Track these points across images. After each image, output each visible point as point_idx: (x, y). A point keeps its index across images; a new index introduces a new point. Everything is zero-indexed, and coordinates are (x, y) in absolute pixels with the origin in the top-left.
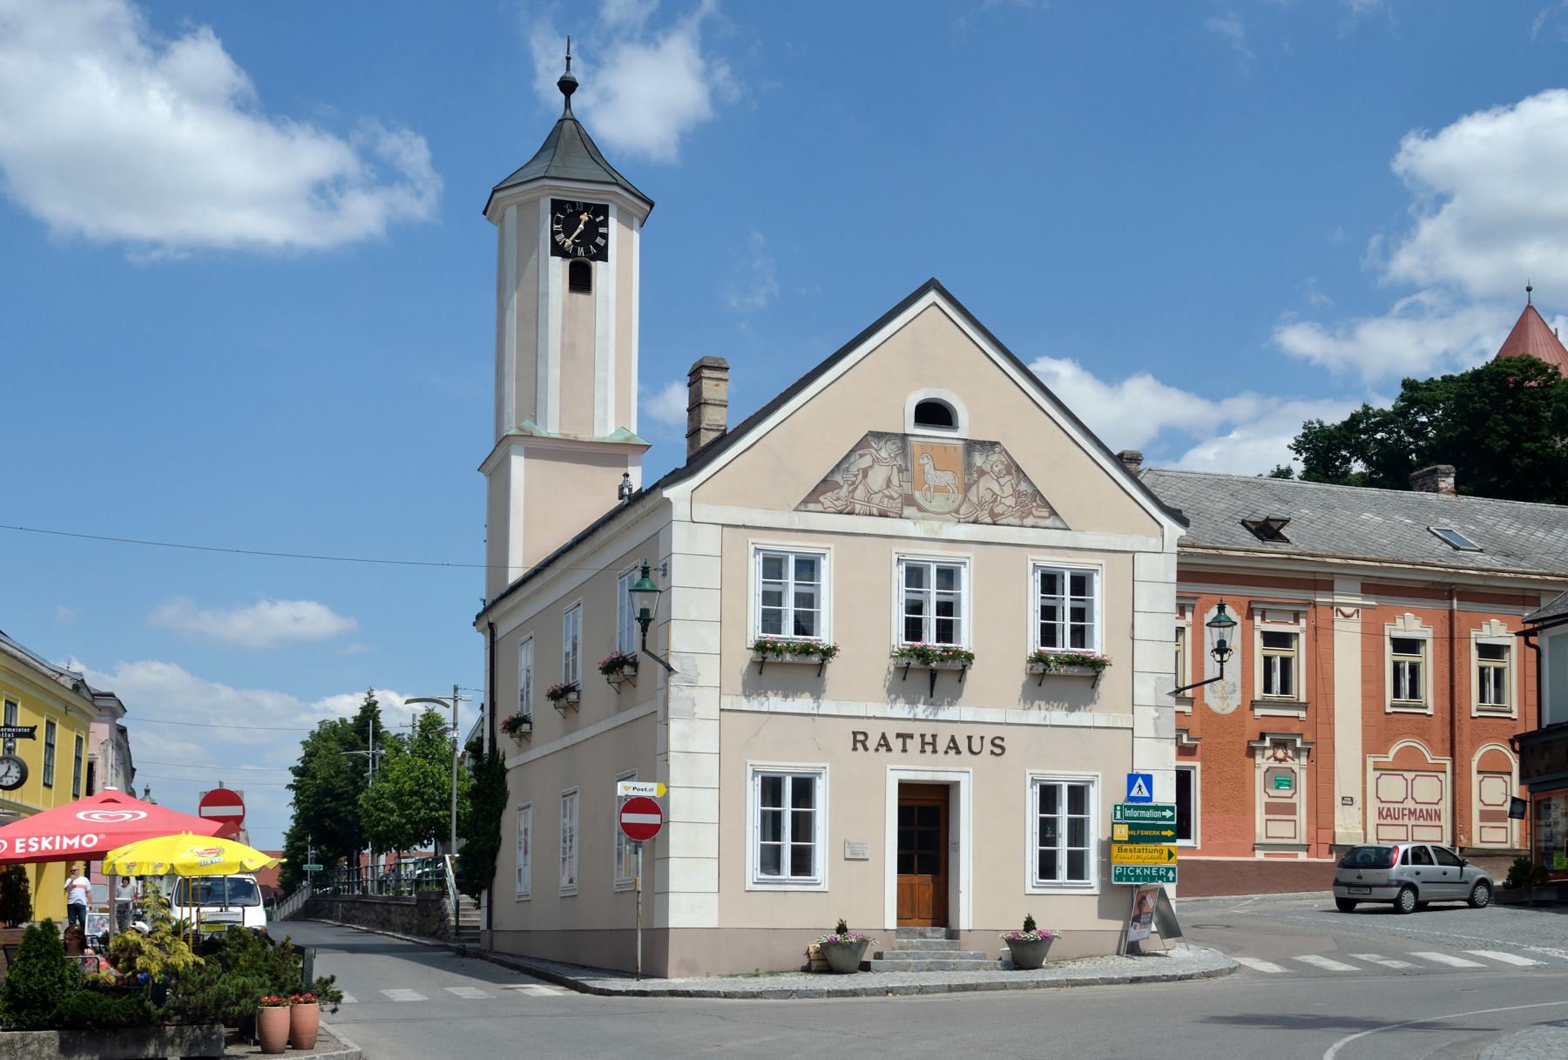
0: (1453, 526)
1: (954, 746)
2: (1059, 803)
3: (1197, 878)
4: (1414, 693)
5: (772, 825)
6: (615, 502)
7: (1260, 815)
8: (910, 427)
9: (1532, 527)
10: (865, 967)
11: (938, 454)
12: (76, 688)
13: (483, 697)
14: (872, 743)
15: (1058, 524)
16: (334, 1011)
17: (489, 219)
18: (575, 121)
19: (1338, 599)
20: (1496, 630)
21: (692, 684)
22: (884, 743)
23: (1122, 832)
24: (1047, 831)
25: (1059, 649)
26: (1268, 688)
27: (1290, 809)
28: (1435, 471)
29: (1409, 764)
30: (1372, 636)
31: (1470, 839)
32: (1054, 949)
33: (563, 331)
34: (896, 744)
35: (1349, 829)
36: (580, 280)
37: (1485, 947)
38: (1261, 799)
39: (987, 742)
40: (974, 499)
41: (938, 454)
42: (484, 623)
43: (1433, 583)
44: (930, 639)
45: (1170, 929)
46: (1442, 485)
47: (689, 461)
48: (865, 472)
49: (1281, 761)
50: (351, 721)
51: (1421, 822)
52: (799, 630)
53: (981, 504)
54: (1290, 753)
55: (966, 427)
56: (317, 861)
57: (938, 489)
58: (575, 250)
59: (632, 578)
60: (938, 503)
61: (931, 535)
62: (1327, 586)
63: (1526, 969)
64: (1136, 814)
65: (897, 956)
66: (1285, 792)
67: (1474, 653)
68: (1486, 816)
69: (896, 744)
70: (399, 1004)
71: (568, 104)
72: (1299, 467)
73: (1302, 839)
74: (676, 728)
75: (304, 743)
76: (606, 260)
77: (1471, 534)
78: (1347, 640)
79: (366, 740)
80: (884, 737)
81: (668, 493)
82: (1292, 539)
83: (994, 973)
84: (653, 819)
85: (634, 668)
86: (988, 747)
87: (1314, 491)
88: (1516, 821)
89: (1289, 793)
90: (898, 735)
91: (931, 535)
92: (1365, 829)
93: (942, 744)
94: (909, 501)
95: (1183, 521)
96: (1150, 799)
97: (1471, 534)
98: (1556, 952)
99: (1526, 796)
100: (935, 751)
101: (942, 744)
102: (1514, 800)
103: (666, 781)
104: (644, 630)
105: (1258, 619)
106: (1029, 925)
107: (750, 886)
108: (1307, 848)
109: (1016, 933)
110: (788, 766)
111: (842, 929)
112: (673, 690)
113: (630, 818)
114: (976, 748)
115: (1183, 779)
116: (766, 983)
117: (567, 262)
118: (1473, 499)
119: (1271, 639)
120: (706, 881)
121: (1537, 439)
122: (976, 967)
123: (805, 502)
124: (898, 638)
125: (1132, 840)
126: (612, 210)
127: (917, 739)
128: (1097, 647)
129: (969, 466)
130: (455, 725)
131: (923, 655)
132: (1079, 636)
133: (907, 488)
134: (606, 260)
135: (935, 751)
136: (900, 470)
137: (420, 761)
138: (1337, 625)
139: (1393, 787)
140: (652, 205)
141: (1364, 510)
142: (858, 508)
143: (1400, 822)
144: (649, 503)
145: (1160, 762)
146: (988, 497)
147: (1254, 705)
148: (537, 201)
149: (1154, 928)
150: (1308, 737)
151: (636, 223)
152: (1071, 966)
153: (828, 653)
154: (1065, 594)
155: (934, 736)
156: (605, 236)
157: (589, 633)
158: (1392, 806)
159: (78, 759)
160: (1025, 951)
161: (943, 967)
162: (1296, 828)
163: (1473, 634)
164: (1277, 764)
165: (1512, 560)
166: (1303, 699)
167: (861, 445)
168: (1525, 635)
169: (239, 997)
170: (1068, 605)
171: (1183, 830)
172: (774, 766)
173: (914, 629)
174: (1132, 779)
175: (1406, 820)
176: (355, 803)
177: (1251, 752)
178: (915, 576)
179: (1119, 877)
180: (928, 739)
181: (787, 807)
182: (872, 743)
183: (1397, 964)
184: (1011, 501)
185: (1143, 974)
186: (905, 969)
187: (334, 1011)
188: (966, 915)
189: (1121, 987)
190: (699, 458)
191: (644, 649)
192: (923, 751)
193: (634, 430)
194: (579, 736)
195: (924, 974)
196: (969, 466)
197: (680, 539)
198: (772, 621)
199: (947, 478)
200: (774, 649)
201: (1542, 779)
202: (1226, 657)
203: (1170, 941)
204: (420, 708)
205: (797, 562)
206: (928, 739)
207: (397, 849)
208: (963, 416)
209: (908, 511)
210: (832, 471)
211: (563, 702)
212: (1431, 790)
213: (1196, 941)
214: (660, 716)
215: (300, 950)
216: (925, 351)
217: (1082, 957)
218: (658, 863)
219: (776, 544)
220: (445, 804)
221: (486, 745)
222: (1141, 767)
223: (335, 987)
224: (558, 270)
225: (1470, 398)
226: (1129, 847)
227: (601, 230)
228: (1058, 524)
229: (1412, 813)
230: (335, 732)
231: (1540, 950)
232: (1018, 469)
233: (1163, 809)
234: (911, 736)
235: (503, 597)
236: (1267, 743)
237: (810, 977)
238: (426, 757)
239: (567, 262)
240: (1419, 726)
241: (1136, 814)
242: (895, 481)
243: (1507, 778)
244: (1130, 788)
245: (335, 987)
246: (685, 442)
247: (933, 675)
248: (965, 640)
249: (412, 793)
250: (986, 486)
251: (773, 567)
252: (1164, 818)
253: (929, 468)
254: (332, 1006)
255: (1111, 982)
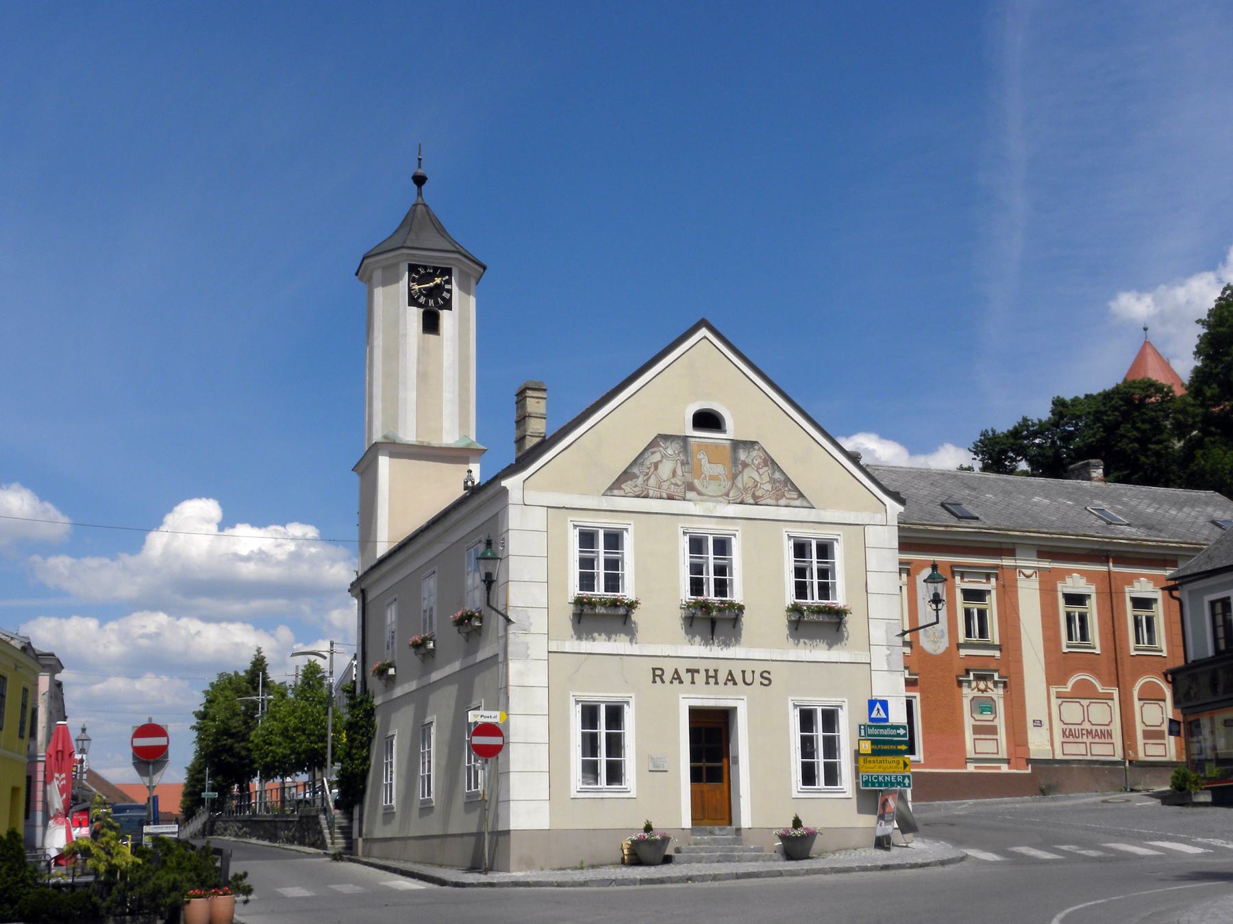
0: (1105, 506)
1: (731, 678)
2: (816, 724)
3: (929, 787)
4: (1084, 636)
5: (590, 744)
6: (460, 492)
7: (969, 735)
8: (689, 431)
9: (1166, 507)
10: (667, 860)
11: (713, 452)
12: (24, 649)
13: (355, 648)
14: (668, 676)
15: (805, 504)
16: (246, 902)
17: (361, 279)
18: (426, 206)
19: (1020, 563)
20: (1145, 584)
21: (526, 631)
22: (677, 677)
23: (866, 747)
24: (807, 746)
25: (809, 601)
26: (968, 634)
27: (993, 730)
28: (1088, 465)
29: (1083, 693)
30: (1047, 592)
31: (1136, 753)
32: (817, 845)
33: (418, 360)
34: (686, 677)
35: (1039, 744)
36: (431, 324)
37: (1161, 839)
38: (968, 723)
39: (757, 675)
40: (740, 485)
41: (713, 452)
42: (358, 590)
43: (1093, 550)
44: (710, 595)
45: (907, 826)
46: (1094, 475)
47: (517, 460)
48: (656, 465)
49: (983, 691)
50: (242, 674)
51: (1097, 740)
52: (314, 761)
53: (745, 489)
54: (990, 685)
55: (732, 430)
56: (213, 789)
57: (713, 478)
58: (427, 302)
59: (476, 551)
60: (713, 488)
61: (709, 513)
62: (1008, 551)
63: (1197, 856)
64: (876, 732)
65: (692, 851)
66: (988, 716)
67: (1129, 604)
68: (1148, 735)
69: (686, 677)
70: (292, 898)
71: (420, 194)
72: (978, 465)
73: (1003, 754)
74: (514, 667)
75: (206, 693)
76: (450, 309)
77: (1120, 512)
78: (1029, 595)
79: (256, 689)
80: (676, 672)
81: (504, 483)
82: (981, 518)
83: (771, 863)
84: (495, 741)
85: (478, 625)
86: (758, 679)
87: (995, 481)
88: (1172, 738)
89: (991, 717)
90: (688, 671)
91: (709, 513)
92: (1052, 745)
93: (722, 677)
94: (690, 487)
95: (902, 501)
96: (887, 720)
97: (1120, 512)
98: (1218, 842)
99: (1180, 718)
100: (717, 683)
101: (722, 677)
102: (1171, 721)
103: (506, 708)
104: (489, 588)
105: (958, 578)
106: (797, 823)
107: (574, 794)
108: (1008, 761)
109: (786, 830)
110: (602, 696)
111: (648, 828)
112: (511, 637)
113: (478, 740)
114: (749, 680)
115: (909, 705)
116: (590, 874)
117: (421, 310)
118: (1118, 485)
119: (970, 595)
120: (539, 791)
121: (1159, 442)
122: (756, 859)
123: (611, 488)
124: (685, 594)
125: (875, 753)
126: (455, 272)
127: (703, 673)
128: (839, 599)
129: (735, 460)
130: (331, 673)
131: (705, 606)
132: (825, 591)
133: (689, 477)
134: (450, 309)
135: (717, 683)
136: (683, 464)
137: (303, 703)
138: (1020, 584)
139: (1073, 712)
140: (484, 268)
141: (1034, 494)
142: (651, 493)
143: (1080, 740)
144: (491, 491)
145: (891, 687)
146: (751, 484)
147: (959, 646)
148: (397, 265)
149: (896, 826)
150: (1004, 671)
151: (473, 282)
152: (831, 857)
153: (632, 606)
154: (814, 557)
155: (716, 671)
156: (450, 291)
157: (437, 598)
158: (1073, 727)
159: (24, 706)
160: (796, 844)
161: (728, 859)
162: (1000, 745)
163: (1127, 589)
164: (980, 694)
165: (1153, 532)
166: (997, 642)
167: (653, 444)
168: (1169, 590)
169: (170, 890)
170: (815, 567)
171: (912, 751)
172: (592, 696)
173: (697, 586)
174: (872, 704)
175: (1085, 739)
176: (248, 740)
177: (960, 684)
178: (697, 545)
179: (866, 783)
180: (711, 673)
181: (603, 729)
182: (668, 676)
183: (1093, 853)
184: (768, 487)
185: (891, 863)
186: (699, 861)
187: (246, 902)
188: (746, 818)
189: (873, 873)
190: (524, 460)
191: (488, 604)
192: (707, 683)
193: (473, 437)
194: (435, 676)
195: (715, 865)
196: (735, 460)
197: (516, 518)
198: (587, 581)
199: (719, 469)
200: (591, 604)
201: (1190, 704)
202: (940, 606)
203: (909, 836)
204: (302, 661)
205: (605, 535)
206: (711, 673)
207: (282, 777)
208: (729, 423)
209: (690, 495)
210: (631, 465)
211: (422, 650)
212: (1104, 714)
213: (929, 836)
214: (501, 659)
215: (218, 852)
216: (701, 372)
217: (839, 850)
218: (499, 777)
219: (590, 521)
220: (323, 738)
221: (358, 687)
222: (878, 694)
223: (246, 882)
224: (414, 316)
225: (1105, 413)
226: (872, 759)
227: (447, 287)
228: (805, 504)
229: (1089, 733)
230: (230, 683)
231: (1205, 840)
232: (773, 462)
233: (897, 727)
234: (698, 671)
235: (373, 568)
236: (971, 677)
237: (624, 869)
238: (307, 700)
239: (421, 310)
240: (1089, 663)
241: (876, 732)
242: (679, 472)
243: (1162, 703)
244: (871, 712)
245: (246, 882)
246: (514, 446)
247: (713, 622)
248: (737, 594)
249: (296, 729)
250: (749, 475)
251: (587, 539)
252: (898, 735)
253: (705, 462)
254: (242, 897)
255: (865, 869)
